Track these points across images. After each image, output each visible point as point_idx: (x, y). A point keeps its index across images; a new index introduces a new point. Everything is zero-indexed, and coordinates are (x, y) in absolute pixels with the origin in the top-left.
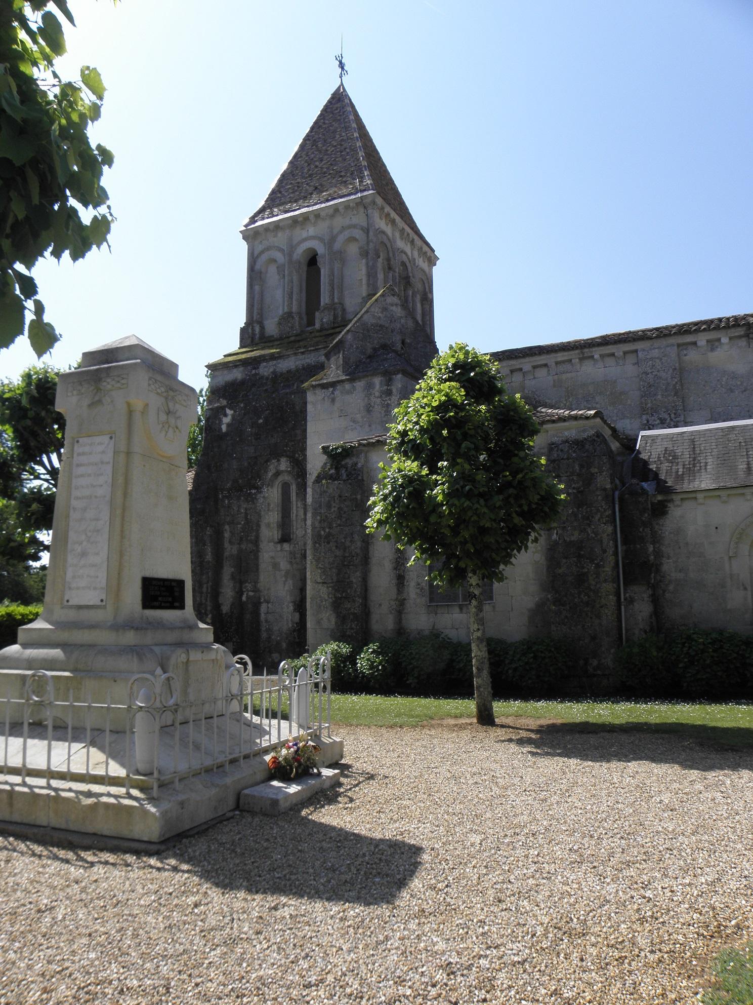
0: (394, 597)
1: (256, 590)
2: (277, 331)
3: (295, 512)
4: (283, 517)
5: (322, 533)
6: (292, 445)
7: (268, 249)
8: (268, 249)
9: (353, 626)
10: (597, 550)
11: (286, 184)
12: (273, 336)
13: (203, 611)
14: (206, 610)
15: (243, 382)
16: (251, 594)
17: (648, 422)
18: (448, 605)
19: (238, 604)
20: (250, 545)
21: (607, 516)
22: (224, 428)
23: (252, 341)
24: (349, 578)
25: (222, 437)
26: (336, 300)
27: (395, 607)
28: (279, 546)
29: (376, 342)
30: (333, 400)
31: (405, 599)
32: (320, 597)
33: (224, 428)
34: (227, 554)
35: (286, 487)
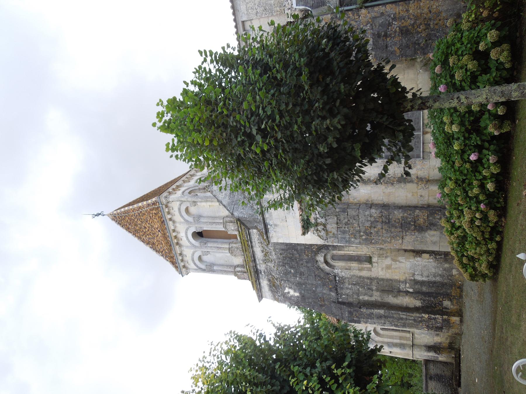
0: (415, 185)
1: (405, 282)
2: (240, 257)
3: (351, 252)
4: (355, 261)
5: (364, 237)
6: (308, 252)
7: (193, 260)
8: (193, 260)
9: (438, 217)
10: (381, 20)
11: (158, 248)
12: (243, 260)
13: (420, 319)
14: (419, 317)
15: (269, 280)
16: (408, 285)
17: (289, 9)
18: (423, 152)
19: (416, 294)
20: (373, 284)
21: (353, 15)
22: (297, 294)
23: (245, 272)
24: (399, 219)
25: (303, 297)
26: (222, 221)
27: (423, 185)
28: (374, 264)
29: (240, 197)
30: (276, 225)
31: (417, 177)
32: (414, 241)
33: (297, 294)
34: (379, 299)
35: (333, 258)
